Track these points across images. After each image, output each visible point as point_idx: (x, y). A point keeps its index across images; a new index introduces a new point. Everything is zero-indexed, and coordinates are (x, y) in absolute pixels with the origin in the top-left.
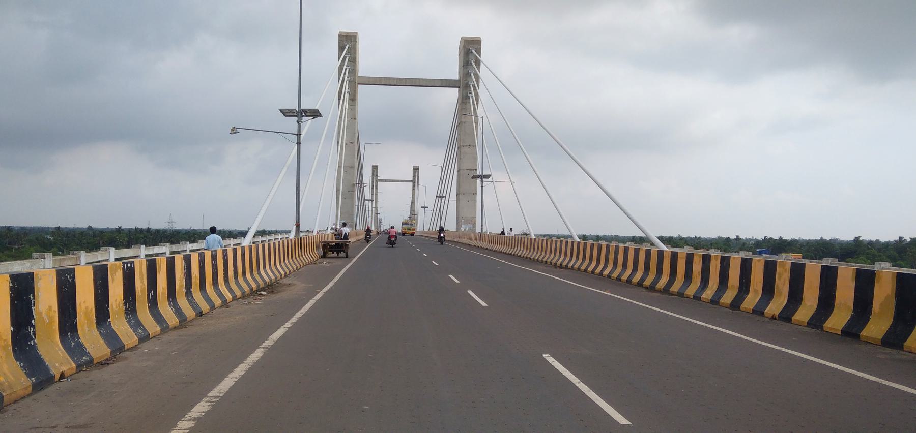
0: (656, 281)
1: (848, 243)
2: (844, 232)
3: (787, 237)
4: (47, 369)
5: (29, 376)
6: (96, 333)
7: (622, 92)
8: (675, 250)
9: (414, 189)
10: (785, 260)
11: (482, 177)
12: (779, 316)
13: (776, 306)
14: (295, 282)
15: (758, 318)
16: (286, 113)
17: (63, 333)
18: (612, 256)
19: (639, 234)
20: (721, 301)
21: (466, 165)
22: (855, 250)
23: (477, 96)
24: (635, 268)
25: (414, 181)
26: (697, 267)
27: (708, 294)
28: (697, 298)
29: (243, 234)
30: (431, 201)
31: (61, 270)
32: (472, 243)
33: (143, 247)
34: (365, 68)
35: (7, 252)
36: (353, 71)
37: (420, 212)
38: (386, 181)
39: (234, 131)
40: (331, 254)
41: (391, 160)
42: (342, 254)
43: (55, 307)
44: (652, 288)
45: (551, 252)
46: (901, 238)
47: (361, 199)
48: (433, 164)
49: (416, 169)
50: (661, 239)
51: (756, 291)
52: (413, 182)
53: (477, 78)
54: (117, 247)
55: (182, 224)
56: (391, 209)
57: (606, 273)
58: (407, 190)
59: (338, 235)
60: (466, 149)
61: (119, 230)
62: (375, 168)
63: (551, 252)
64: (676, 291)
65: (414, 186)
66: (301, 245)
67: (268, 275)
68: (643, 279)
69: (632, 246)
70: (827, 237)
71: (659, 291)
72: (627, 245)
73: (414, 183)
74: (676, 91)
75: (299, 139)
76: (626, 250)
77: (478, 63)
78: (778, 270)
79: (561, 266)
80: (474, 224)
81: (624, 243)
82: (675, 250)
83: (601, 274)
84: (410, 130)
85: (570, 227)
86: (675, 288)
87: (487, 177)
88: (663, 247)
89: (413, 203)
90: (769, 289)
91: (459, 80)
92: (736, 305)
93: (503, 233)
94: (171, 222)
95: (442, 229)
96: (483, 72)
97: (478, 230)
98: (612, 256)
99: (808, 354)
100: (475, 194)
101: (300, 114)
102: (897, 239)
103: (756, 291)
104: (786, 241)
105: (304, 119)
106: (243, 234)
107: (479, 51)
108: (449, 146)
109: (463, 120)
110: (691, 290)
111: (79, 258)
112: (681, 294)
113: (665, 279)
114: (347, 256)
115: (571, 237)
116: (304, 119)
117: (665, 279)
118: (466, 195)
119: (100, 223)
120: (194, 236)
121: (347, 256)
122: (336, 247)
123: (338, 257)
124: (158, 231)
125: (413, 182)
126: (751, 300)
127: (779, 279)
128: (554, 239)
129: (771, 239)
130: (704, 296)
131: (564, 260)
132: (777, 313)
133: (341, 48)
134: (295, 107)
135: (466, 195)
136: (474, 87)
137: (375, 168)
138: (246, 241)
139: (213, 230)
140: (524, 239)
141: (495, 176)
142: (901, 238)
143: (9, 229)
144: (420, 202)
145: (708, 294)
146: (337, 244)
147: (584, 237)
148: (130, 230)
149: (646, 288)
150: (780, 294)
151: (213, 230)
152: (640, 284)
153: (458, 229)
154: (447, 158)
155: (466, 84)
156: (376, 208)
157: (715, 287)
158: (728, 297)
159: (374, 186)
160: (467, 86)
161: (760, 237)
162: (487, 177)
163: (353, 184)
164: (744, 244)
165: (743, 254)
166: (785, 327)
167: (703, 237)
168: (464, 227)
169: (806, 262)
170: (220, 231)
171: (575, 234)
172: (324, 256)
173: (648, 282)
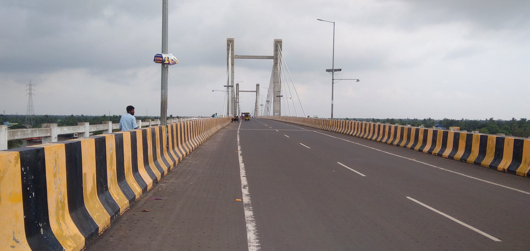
0: (377, 138)
2: (504, 115)
7: (354, 40)
10: (377, 124)
12: (490, 166)
18: (376, 130)
24: (354, 131)
25: (257, 91)
26: (421, 136)
30: (264, 103)
31: (105, 139)
37: (260, 108)
38: (243, 91)
49: (258, 85)
56: (246, 105)
62: (237, 85)
65: (276, 64)
66: (229, 119)
69: (372, 124)
74: (385, 39)
76: (396, 128)
81: (394, 124)
89: (256, 102)
90: (468, 149)
98: (376, 130)
122: (235, 119)
125: (256, 92)
128: (364, 122)
131: (360, 134)
133: (228, 45)
142: (513, 119)
144: (259, 103)
149: (504, 171)
152: (392, 144)
157: (509, 162)
161: (442, 119)
165: (409, 126)
167: (419, 119)
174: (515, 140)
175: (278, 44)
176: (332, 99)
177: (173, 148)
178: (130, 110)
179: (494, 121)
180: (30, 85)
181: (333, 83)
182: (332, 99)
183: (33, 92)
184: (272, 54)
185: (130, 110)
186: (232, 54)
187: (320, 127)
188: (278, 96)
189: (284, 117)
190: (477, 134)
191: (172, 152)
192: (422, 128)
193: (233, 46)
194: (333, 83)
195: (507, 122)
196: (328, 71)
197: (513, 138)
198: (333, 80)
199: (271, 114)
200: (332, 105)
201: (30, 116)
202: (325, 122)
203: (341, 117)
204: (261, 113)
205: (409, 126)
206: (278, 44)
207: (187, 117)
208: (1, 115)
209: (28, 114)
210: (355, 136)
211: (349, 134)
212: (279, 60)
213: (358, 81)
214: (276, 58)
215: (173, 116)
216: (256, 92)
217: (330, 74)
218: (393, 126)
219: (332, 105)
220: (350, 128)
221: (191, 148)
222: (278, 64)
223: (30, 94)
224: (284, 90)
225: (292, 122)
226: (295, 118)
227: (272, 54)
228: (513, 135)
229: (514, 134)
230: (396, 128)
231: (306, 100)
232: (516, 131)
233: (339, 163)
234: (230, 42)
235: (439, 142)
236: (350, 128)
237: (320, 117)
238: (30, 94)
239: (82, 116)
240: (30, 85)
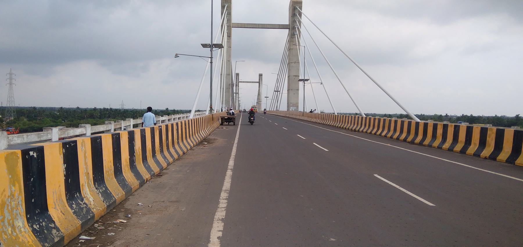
1: (512, 118)
3: (475, 114)
4: (142, 178)
5: (138, 180)
6: (153, 161)
8: (410, 120)
9: (259, 87)
11: (304, 80)
13: (487, 152)
14: (216, 138)
15: (477, 158)
16: (204, 46)
17: (143, 162)
19: (405, 113)
21: (293, 73)
23: (300, 32)
26: (440, 131)
27: (447, 145)
28: (439, 148)
29: (190, 111)
32: (298, 117)
33: (132, 119)
34: (235, 19)
35: (34, 121)
36: (229, 20)
37: (263, 100)
39: (177, 56)
40: (225, 123)
41: (247, 71)
42: (232, 123)
43: (140, 148)
44: (412, 142)
45: (348, 123)
48: (272, 74)
49: (261, 75)
50: (417, 116)
51: (475, 144)
53: (300, 22)
54: (134, 119)
55: (129, 106)
56: (246, 99)
57: (384, 134)
58: (259, 87)
59: (228, 113)
60: (293, 64)
61: (95, 109)
62: (237, 75)
63: (348, 123)
64: (427, 144)
65: (259, 85)
66: (212, 118)
67: (203, 134)
68: (406, 138)
70: (499, 115)
71: (416, 144)
72: (403, 119)
73: (259, 83)
75: (211, 60)
77: (300, 14)
78: (489, 132)
79: (355, 131)
80: (298, 107)
82: (410, 120)
83: (380, 135)
84: (255, 53)
85: (359, 108)
86: (427, 142)
87: (307, 80)
88: (418, 120)
89: (259, 94)
91: (289, 25)
92: (463, 151)
93: (311, 112)
94: (123, 105)
95: (265, 110)
96: (303, 19)
97: (301, 109)
99: (511, 176)
100: (298, 90)
101: (212, 46)
103: (475, 144)
104: (475, 117)
105: (214, 49)
106: (190, 111)
107: (301, 8)
108: (282, 62)
109: (292, 48)
110: (436, 144)
111: (121, 124)
112: (430, 146)
113: (397, 134)
114: (234, 124)
115: (361, 115)
116: (214, 49)
117: (397, 134)
118: (293, 90)
119: (116, 105)
120: (136, 114)
121: (234, 124)
122: (229, 120)
123: (229, 125)
124: (116, 110)
125: (259, 83)
126: (473, 149)
127: (489, 137)
128: (431, 123)
129: (466, 116)
130: (444, 147)
132: (488, 155)
134: (209, 42)
135: (293, 90)
136: (298, 28)
138: (191, 116)
139: (150, 109)
140: (332, 116)
141: (312, 80)
143: (34, 108)
145: (447, 145)
146: (229, 118)
147: (367, 115)
148: (100, 109)
149: (409, 142)
150: (490, 145)
151: (150, 109)
153: (288, 110)
154: (281, 70)
155: (293, 27)
157: (451, 142)
158: (458, 147)
159: (237, 85)
160: (294, 28)
162: (307, 80)
163: (231, 86)
164: (450, 119)
165: (378, 117)
166: (494, 163)
168: (291, 109)
170: (156, 111)
171: (364, 112)
172: (222, 124)
177: (162, 151)
191: (189, 140)
201: (11, 107)
203: (342, 112)
209: (8, 106)
211: (343, 128)
216: (259, 83)
221: (197, 141)
223: (11, 84)
233: (431, 204)
238: (11, 84)
239: (78, 108)
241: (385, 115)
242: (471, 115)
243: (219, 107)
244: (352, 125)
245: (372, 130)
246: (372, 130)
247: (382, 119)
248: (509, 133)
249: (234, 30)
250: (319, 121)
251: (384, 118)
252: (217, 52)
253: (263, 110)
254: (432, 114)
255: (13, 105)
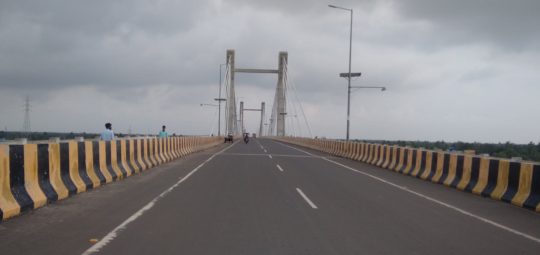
0: (382, 163)
10: (420, 150)
20: (433, 179)
22: (508, 149)
25: (262, 110)
26: (429, 161)
30: (269, 122)
34: (237, 66)
36: (232, 67)
39: (201, 105)
45: (356, 152)
46: (531, 142)
47: (235, 119)
49: (263, 104)
52: (262, 110)
56: (251, 124)
59: (229, 136)
62: (242, 103)
63: (356, 152)
65: (280, 78)
66: (219, 138)
76: (406, 152)
79: (340, 157)
81: (432, 149)
89: (262, 121)
101: (220, 100)
102: (529, 143)
113: (400, 166)
117: (375, 159)
122: (229, 139)
125: (262, 110)
131: (352, 155)
133: (228, 57)
137: (242, 103)
142: (531, 142)
156: (242, 124)
157: (402, 165)
165: (379, 145)
169: (479, 156)
173: (391, 167)
174: (473, 158)
175: (283, 57)
176: (348, 114)
178: (108, 126)
179: (319, 140)
180: (27, 101)
181: (349, 92)
182: (348, 114)
183: (30, 108)
184: (277, 68)
185: (108, 126)
186: (232, 67)
187: (331, 151)
188: (282, 114)
189: (288, 138)
190: (486, 157)
192: (363, 144)
193: (233, 59)
194: (349, 92)
195: (524, 146)
196: (342, 75)
197: (532, 164)
198: (349, 87)
199: (275, 134)
200: (348, 121)
201: (27, 133)
202: (338, 144)
204: (265, 133)
205: (379, 145)
206: (283, 57)
207: (143, 136)
208: (2, 132)
209: (24, 131)
210: (387, 168)
212: (284, 74)
213: (384, 89)
214: (280, 72)
215: (176, 135)
217: (345, 80)
218: (403, 149)
219: (348, 121)
220: (376, 155)
222: (283, 79)
223: (27, 110)
224: (290, 107)
225: (296, 143)
226: (299, 139)
227: (277, 68)
228: (532, 160)
229: (534, 159)
230: (406, 152)
231: (313, 120)
232: (536, 156)
234: (230, 54)
235: (524, 179)
236: (376, 155)
237: (328, 137)
239: (443, 142)
240: (27, 101)
241: (384, 142)
242: (500, 143)
243: (224, 133)
244: (357, 155)
245: (363, 158)
246: (363, 158)
247: (382, 147)
248: (527, 167)
249: (236, 74)
250: (317, 148)
251: (385, 145)
252: (223, 103)
253: (241, 134)
254: (396, 140)
255: (29, 131)
